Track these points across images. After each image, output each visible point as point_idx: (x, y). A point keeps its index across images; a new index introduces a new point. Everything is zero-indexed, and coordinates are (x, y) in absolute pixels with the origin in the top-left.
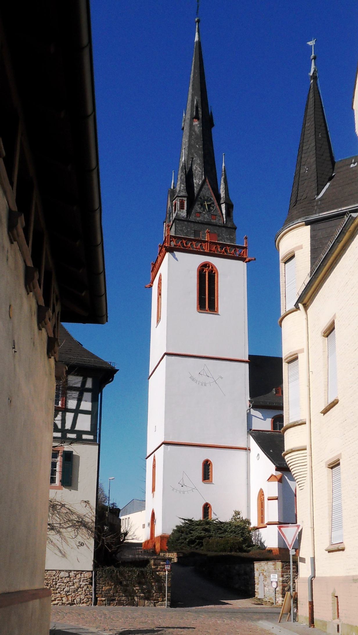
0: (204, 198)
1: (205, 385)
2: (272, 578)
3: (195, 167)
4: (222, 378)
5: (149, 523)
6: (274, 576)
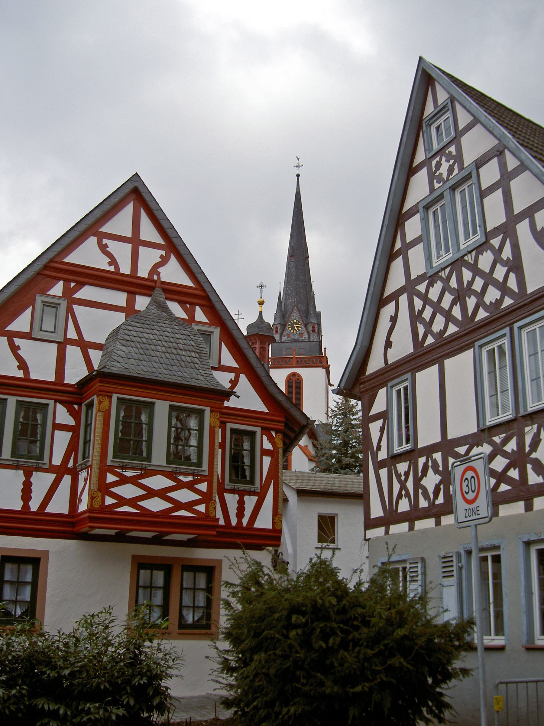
0: (294, 321)
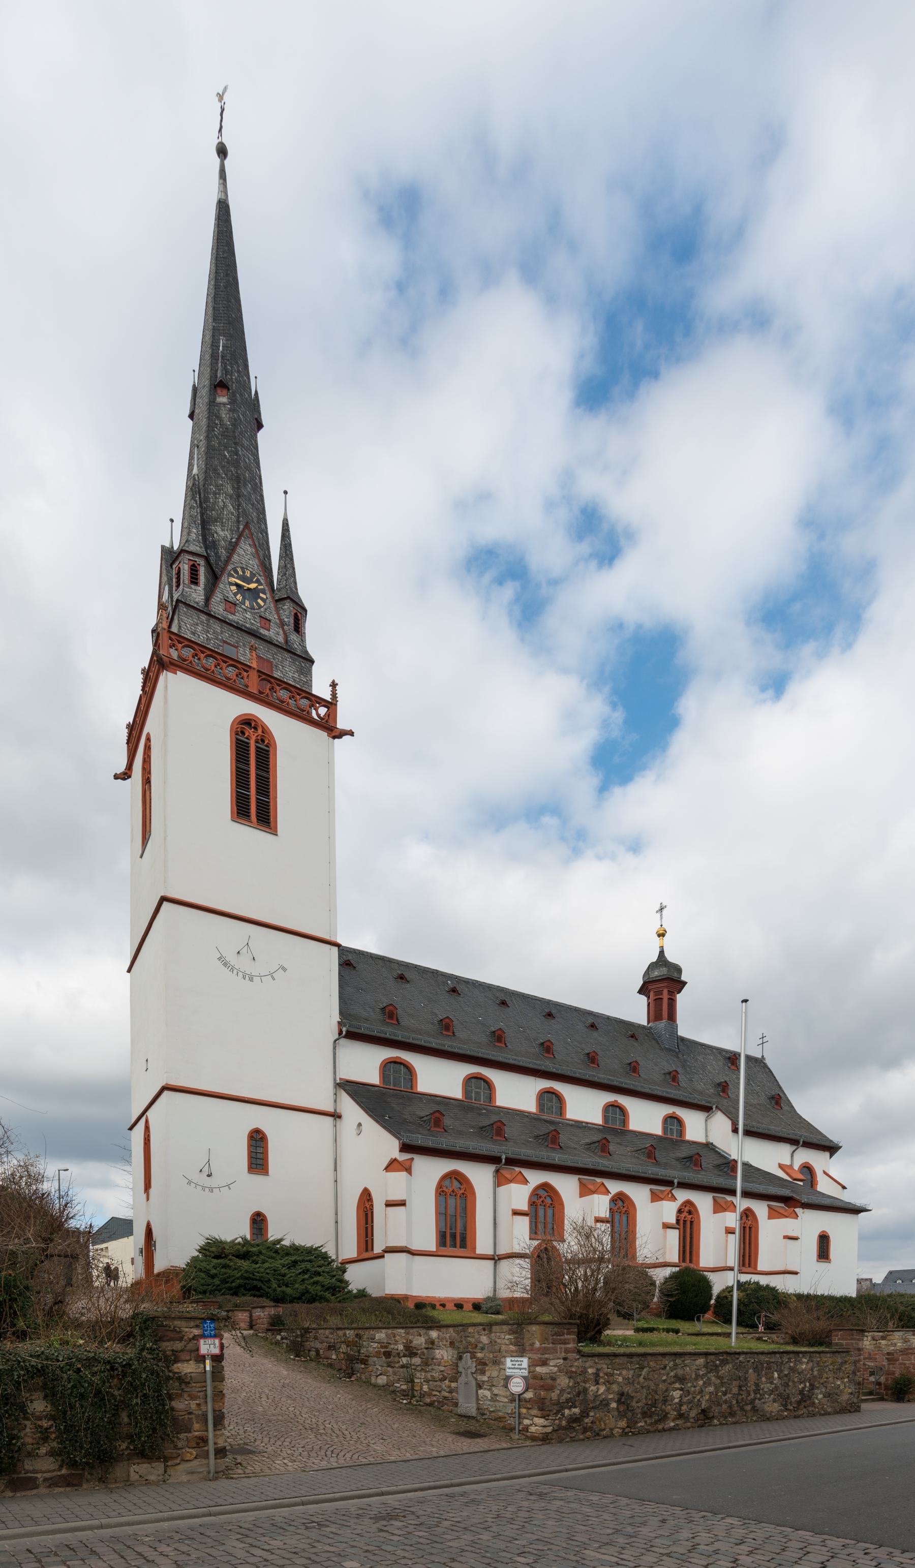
0: (244, 572)
1: (251, 980)
2: (510, 1368)
3: (222, 500)
4: (285, 970)
5: (142, 1249)
6: (517, 1361)
